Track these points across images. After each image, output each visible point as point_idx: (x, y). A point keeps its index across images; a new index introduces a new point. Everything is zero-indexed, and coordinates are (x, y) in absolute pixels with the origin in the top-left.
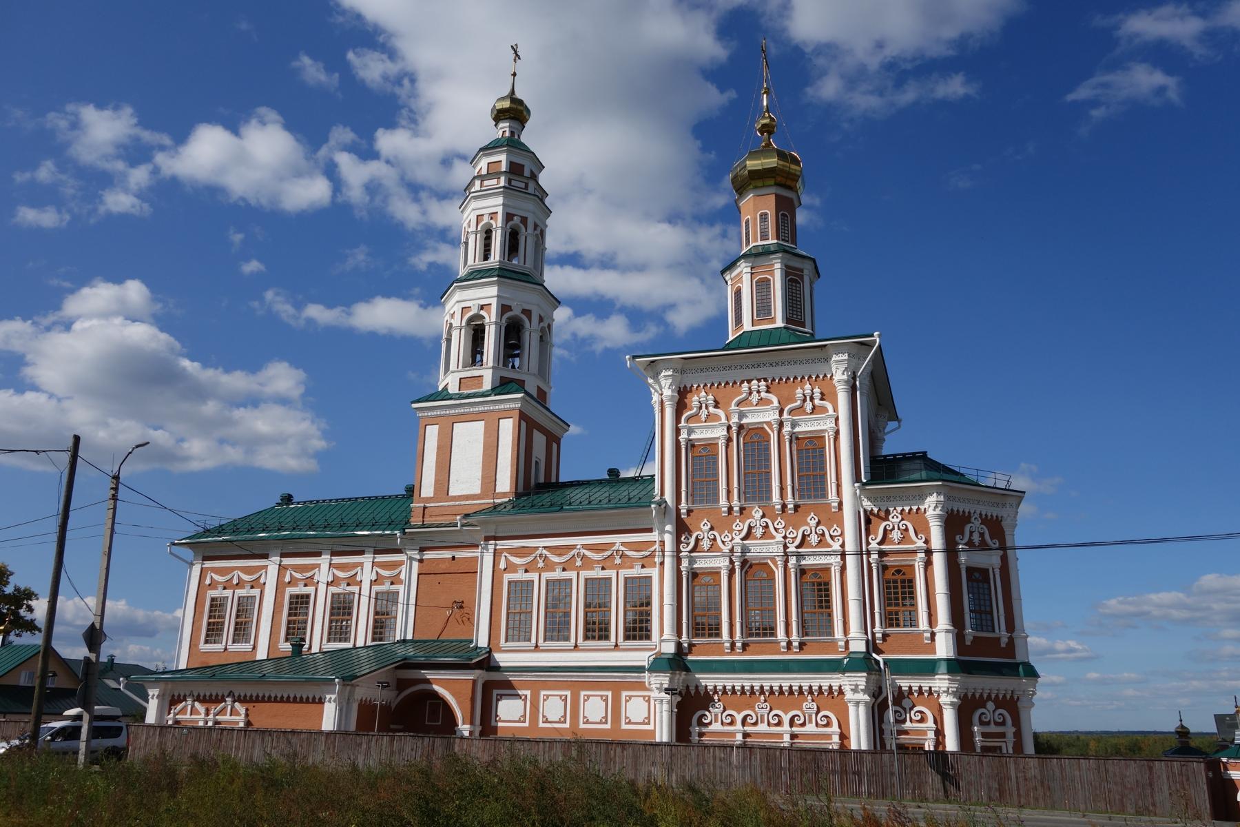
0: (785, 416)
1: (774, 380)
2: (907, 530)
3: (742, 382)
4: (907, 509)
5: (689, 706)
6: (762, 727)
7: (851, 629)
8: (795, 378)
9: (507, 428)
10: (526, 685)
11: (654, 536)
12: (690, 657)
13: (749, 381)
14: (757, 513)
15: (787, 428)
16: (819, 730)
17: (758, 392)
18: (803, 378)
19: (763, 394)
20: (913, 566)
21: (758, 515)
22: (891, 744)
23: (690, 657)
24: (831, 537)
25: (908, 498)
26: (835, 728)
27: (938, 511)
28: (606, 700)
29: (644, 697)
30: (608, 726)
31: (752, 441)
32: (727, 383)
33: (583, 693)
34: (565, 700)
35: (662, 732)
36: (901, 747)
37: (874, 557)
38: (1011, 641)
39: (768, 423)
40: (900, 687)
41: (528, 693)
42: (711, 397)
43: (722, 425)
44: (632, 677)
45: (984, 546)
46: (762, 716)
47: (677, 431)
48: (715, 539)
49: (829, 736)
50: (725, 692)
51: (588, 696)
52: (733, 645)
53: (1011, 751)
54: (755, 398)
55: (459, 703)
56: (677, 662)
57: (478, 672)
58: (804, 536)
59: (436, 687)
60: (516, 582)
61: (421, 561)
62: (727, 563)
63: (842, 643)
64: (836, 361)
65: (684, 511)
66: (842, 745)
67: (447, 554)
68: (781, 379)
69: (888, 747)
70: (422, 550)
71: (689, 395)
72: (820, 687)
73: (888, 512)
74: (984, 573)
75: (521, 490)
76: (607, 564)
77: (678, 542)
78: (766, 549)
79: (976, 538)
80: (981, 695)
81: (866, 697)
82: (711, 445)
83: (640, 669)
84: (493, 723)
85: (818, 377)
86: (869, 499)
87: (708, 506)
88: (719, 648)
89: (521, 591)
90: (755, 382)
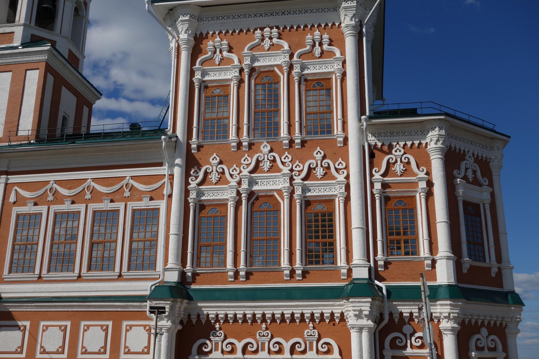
0: (295, 58)
1: (285, 28)
2: (409, 163)
3: (256, 29)
4: (409, 143)
7: (354, 253)
8: (306, 26)
9: (33, 78)
10: (25, 316)
11: (164, 170)
12: (193, 287)
13: (262, 29)
14: (265, 148)
15: (297, 70)
17: (271, 38)
18: (313, 26)
20: (414, 197)
21: (266, 150)
23: (193, 287)
24: (337, 170)
25: (410, 134)
27: (439, 145)
29: (145, 326)
31: (263, 81)
32: (241, 31)
34: (65, 331)
37: (378, 186)
38: (499, 274)
39: (278, 66)
40: (401, 313)
41: (27, 324)
42: (225, 42)
43: (235, 67)
44: (134, 306)
45: (476, 182)
46: (263, 344)
47: (192, 73)
48: (223, 173)
51: (88, 326)
52: (237, 273)
54: (267, 43)
56: (181, 290)
58: (310, 169)
60: (24, 215)
62: (234, 194)
63: (344, 271)
64: (345, 8)
65: (194, 146)
71: (204, 41)
72: (322, 314)
73: (391, 147)
74: (476, 206)
75: (44, 133)
77: (187, 175)
78: (272, 183)
79: (470, 175)
80: (476, 322)
81: (370, 323)
82: (224, 85)
85: (327, 25)
86: (373, 135)
87: (216, 142)
88: (222, 276)
90: (267, 29)
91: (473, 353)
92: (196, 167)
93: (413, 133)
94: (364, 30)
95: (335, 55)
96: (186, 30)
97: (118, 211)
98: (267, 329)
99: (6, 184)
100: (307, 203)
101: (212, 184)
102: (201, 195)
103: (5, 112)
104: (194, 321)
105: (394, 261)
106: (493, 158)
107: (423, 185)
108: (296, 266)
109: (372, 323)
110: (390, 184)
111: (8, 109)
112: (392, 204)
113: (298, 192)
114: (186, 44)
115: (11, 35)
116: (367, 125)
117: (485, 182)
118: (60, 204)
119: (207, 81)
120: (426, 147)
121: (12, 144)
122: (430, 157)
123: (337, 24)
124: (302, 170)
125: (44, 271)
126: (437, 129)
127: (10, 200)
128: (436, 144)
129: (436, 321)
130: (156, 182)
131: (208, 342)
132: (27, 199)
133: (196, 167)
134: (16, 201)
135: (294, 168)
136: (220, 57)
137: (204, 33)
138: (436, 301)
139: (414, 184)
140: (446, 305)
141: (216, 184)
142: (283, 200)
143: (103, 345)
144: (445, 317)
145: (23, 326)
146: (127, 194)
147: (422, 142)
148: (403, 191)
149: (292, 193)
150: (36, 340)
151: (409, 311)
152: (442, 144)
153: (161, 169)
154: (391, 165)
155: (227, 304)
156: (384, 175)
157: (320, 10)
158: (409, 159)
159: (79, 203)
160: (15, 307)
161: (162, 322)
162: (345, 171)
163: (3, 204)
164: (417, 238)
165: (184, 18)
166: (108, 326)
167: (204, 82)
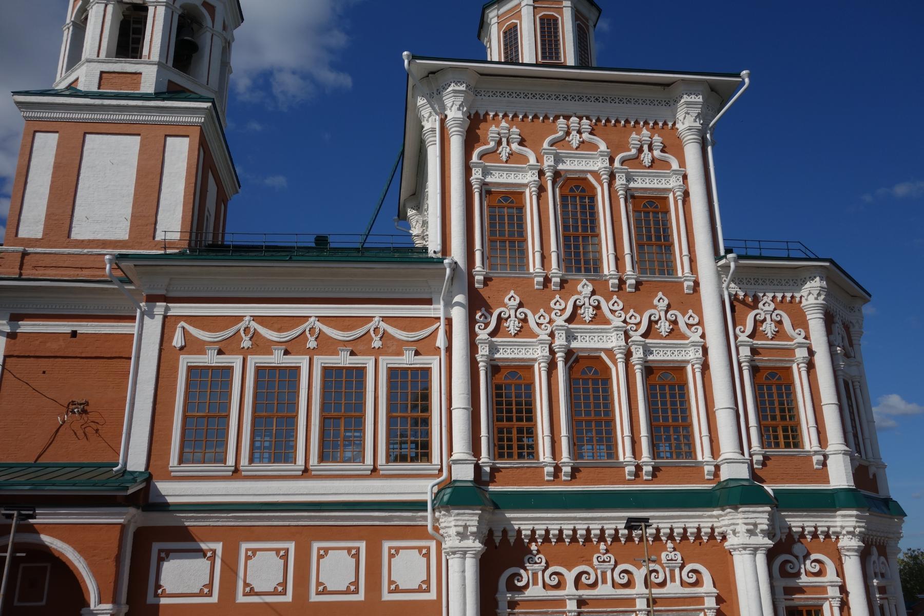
0: (617, 164)
3: (557, 118)
4: (779, 296)
6: (605, 590)
7: (724, 442)
9: (179, 154)
10: (214, 534)
11: (437, 310)
12: (492, 488)
13: (567, 118)
14: (585, 288)
15: (620, 181)
19: (586, 136)
20: (789, 369)
23: (492, 488)
26: (708, 586)
30: (361, 597)
31: (576, 194)
33: (316, 545)
34: (285, 557)
37: (745, 352)
39: (594, 173)
40: (790, 528)
41: (219, 547)
43: (532, 168)
46: (604, 573)
50: (546, 538)
55: (92, 565)
57: (132, 511)
58: (651, 323)
59: (46, 539)
61: (12, 336)
62: (546, 353)
64: (687, 103)
67: (64, 327)
68: (608, 121)
70: (15, 318)
71: (482, 125)
73: (756, 300)
76: (359, 347)
77: (471, 322)
81: (769, 543)
83: (420, 506)
84: (150, 599)
85: (656, 123)
89: (210, 385)
90: (574, 119)
91: (875, 581)
92: (483, 309)
93: (783, 282)
94: (708, 136)
95: (529, 161)
96: (460, 105)
97: (230, 369)
98: (607, 551)
99: (165, 317)
100: (495, 368)
101: (510, 336)
102: (494, 351)
103: (131, 199)
105: (773, 455)
106: (854, 321)
108: (643, 460)
109: (480, 545)
110: (760, 350)
111: (135, 194)
112: (763, 375)
114: (461, 126)
115: (135, 76)
116: (736, 267)
118: (264, 354)
119: (491, 183)
120: (800, 302)
121: (168, 251)
122: (806, 316)
123: (670, 124)
124: (640, 323)
125: (314, 460)
126: (818, 279)
127: (174, 343)
128: (816, 299)
129: (834, 538)
130: (422, 328)
131: (522, 572)
132: (204, 342)
133: (483, 309)
134: (185, 346)
135: (628, 320)
136: (508, 150)
137: (482, 113)
138: (836, 511)
139: (790, 351)
140: (851, 516)
141: (515, 335)
142: (616, 365)
143: (353, 580)
144: (849, 533)
145: (211, 550)
146: (377, 343)
147: (796, 294)
148: (776, 360)
149: (628, 354)
150: (235, 573)
151: (614, 526)
152: (824, 300)
153: (430, 309)
154: (758, 323)
155: (549, 515)
156: (752, 336)
157: (648, 102)
158: (526, 315)
159: (298, 353)
160: (196, 518)
161: (466, 541)
162: (700, 329)
163: (160, 350)
164: (799, 424)
165: (457, 88)
166: (287, 550)
167: (630, 189)
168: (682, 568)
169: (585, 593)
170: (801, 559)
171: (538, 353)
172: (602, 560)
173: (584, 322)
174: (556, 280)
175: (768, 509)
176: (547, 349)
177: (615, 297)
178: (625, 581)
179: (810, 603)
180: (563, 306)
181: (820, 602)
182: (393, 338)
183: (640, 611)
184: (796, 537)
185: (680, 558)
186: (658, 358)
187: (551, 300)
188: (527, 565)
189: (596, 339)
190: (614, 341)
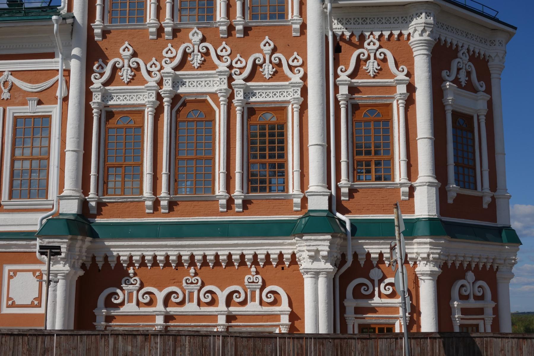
2: (385, 60)
4: (386, 34)
5: (95, 283)
6: (191, 307)
7: (310, 178)
11: (57, 63)
12: (98, 220)
16: (262, 309)
20: (390, 105)
22: (353, 324)
23: (98, 220)
24: (291, 68)
25: (388, 21)
26: (285, 306)
27: (426, 36)
28: (40, 277)
31: (189, 113)
35: (56, 320)
36: (364, 328)
37: (344, 90)
38: (493, 205)
40: (369, 254)
45: (470, 87)
46: (191, 293)
48: (138, 69)
49: (276, 317)
52: (156, 204)
53: (489, 330)
56: (82, 224)
58: (255, 66)
62: (153, 98)
65: (97, 31)
66: (292, 328)
69: (350, 331)
72: (268, 256)
73: (362, 38)
77: (89, 71)
80: (461, 264)
81: (329, 266)
86: (340, 21)
88: (137, 206)
91: (456, 303)
92: (100, 60)
93: (392, 21)
100: (251, 111)
101: (123, 84)
104: (362, 263)
105: (361, 188)
106: (493, 55)
107: (402, 89)
109: (331, 267)
112: (361, 114)
113: (239, 96)
117: (481, 86)
120: (408, 39)
124: (245, 67)
126: (423, 15)
128: (421, 35)
129: (411, 263)
130: (46, 80)
131: (119, 291)
133: (100, 60)
135: (234, 64)
138: (413, 239)
139: (392, 88)
140: (425, 243)
141: (128, 83)
144: (423, 259)
147: (403, 32)
148: (376, 98)
149: (231, 97)
152: (429, 36)
153: (52, 62)
154: (362, 62)
155: (143, 243)
162: (302, 70)
168: (262, 289)
169: (234, 309)
170: (376, 283)
171: (144, 98)
172: (190, 282)
173: (193, 69)
174: (239, 27)
175: (329, 237)
176: (154, 95)
177: (224, 43)
178: (208, 300)
179: (382, 321)
180: (174, 54)
181: (391, 321)
182: (20, 90)
183: (283, 325)
184: (375, 263)
185: (261, 280)
186: (261, 99)
187: (164, 48)
188: (123, 285)
189: (203, 84)
190: (215, 85)
